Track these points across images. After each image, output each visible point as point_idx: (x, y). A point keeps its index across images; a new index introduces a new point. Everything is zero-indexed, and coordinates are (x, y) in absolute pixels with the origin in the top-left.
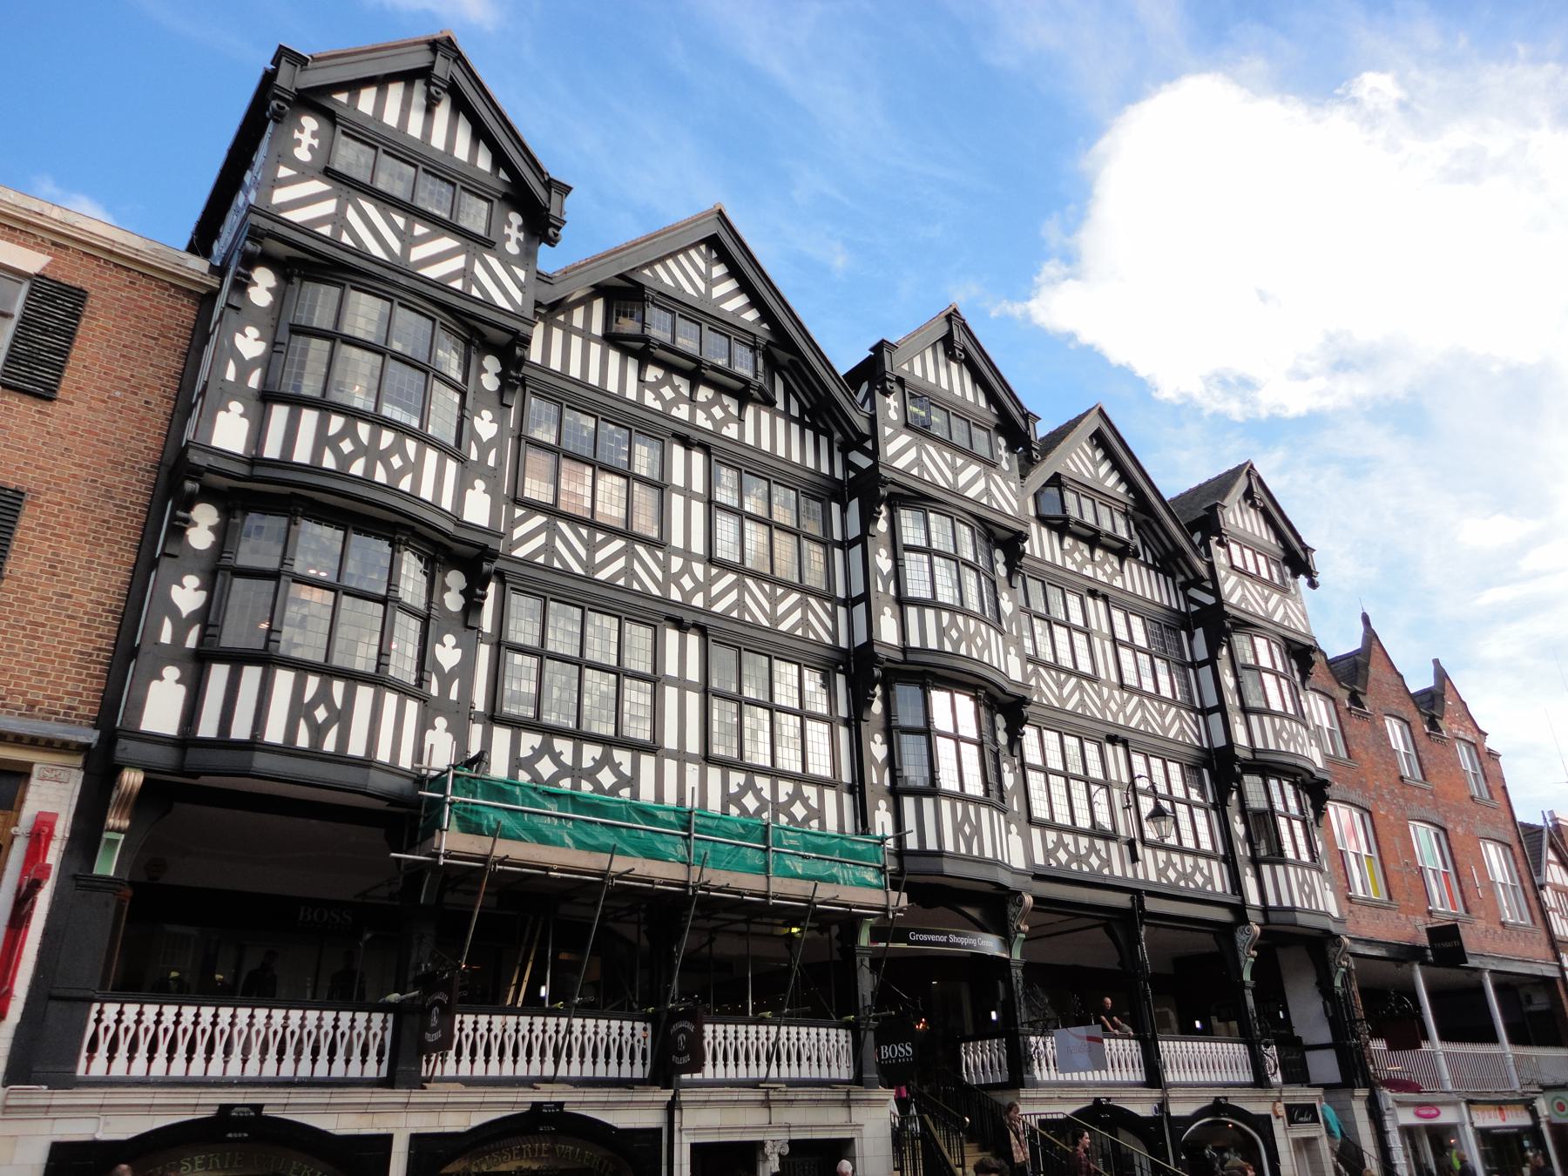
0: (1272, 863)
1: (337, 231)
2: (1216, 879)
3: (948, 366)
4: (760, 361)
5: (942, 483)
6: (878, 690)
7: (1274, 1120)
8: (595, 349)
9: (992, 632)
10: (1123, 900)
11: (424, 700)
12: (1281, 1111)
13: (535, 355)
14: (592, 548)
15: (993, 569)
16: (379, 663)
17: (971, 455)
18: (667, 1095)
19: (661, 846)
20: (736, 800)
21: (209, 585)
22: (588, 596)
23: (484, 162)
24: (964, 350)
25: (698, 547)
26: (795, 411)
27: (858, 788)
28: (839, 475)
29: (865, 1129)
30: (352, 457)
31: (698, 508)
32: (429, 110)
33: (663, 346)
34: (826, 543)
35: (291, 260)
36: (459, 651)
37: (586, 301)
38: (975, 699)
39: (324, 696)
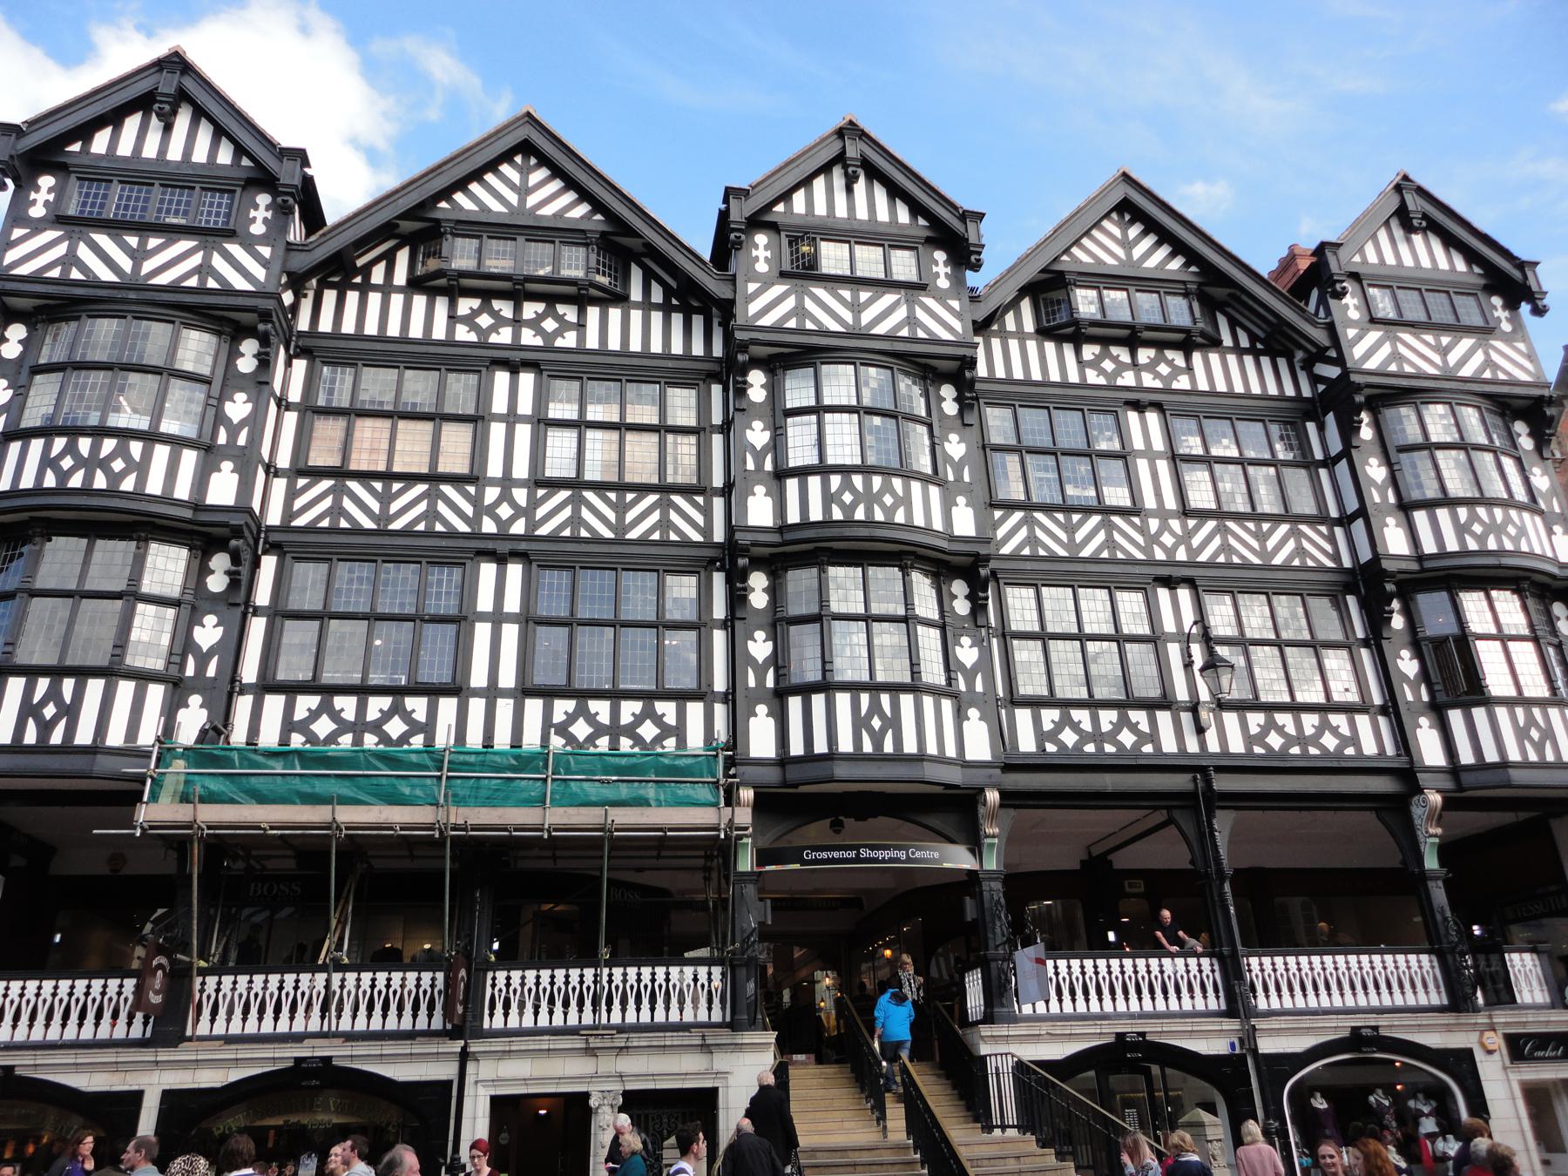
0: (1466, 707)
1: (801, 321)
2: (1371, 737)
3: (1409, 241)
4: (1196, 305)
5: (1432, 371)
6: (1396, 605)
7: (1479, 1056)
8: (1032, 345)
9: (1526, 515)
10: (1181, 782)
11: (955, 696)
12: (1496, 1040)
13: (982, 370)
14: (1071, 529)
15: (1515, 445)
16: (913, 673)
17: (1458, 329)
18: (457, 1046)
19: (407, 791)
20: (1053, 736)
21: (773, 637)
22: (1074, 574)
23: (903, 216)
24: (1425, 216)
25: (1171, 503)
26: (1244, 342)
27: (1391, 708)
28: (1307, 392)
29: (732, 1080)
30: (854, 505)
31: (1163, 466)
32: (849, 190)
33: (1094, 324)
34: (1306, 463)
35: (772, 357)
36: (221, 629)
37: (1014, 304)
38: (1518, 591)
39: (876, 707)
